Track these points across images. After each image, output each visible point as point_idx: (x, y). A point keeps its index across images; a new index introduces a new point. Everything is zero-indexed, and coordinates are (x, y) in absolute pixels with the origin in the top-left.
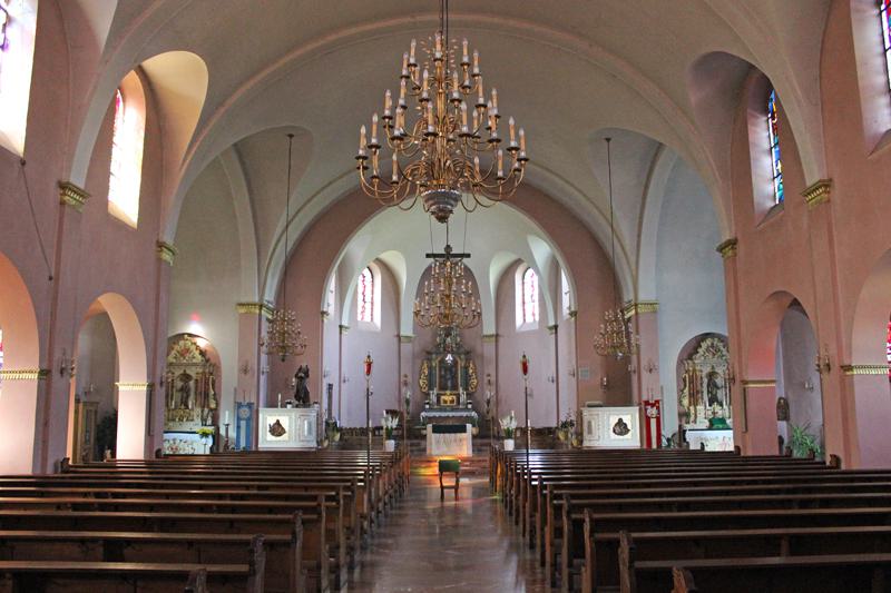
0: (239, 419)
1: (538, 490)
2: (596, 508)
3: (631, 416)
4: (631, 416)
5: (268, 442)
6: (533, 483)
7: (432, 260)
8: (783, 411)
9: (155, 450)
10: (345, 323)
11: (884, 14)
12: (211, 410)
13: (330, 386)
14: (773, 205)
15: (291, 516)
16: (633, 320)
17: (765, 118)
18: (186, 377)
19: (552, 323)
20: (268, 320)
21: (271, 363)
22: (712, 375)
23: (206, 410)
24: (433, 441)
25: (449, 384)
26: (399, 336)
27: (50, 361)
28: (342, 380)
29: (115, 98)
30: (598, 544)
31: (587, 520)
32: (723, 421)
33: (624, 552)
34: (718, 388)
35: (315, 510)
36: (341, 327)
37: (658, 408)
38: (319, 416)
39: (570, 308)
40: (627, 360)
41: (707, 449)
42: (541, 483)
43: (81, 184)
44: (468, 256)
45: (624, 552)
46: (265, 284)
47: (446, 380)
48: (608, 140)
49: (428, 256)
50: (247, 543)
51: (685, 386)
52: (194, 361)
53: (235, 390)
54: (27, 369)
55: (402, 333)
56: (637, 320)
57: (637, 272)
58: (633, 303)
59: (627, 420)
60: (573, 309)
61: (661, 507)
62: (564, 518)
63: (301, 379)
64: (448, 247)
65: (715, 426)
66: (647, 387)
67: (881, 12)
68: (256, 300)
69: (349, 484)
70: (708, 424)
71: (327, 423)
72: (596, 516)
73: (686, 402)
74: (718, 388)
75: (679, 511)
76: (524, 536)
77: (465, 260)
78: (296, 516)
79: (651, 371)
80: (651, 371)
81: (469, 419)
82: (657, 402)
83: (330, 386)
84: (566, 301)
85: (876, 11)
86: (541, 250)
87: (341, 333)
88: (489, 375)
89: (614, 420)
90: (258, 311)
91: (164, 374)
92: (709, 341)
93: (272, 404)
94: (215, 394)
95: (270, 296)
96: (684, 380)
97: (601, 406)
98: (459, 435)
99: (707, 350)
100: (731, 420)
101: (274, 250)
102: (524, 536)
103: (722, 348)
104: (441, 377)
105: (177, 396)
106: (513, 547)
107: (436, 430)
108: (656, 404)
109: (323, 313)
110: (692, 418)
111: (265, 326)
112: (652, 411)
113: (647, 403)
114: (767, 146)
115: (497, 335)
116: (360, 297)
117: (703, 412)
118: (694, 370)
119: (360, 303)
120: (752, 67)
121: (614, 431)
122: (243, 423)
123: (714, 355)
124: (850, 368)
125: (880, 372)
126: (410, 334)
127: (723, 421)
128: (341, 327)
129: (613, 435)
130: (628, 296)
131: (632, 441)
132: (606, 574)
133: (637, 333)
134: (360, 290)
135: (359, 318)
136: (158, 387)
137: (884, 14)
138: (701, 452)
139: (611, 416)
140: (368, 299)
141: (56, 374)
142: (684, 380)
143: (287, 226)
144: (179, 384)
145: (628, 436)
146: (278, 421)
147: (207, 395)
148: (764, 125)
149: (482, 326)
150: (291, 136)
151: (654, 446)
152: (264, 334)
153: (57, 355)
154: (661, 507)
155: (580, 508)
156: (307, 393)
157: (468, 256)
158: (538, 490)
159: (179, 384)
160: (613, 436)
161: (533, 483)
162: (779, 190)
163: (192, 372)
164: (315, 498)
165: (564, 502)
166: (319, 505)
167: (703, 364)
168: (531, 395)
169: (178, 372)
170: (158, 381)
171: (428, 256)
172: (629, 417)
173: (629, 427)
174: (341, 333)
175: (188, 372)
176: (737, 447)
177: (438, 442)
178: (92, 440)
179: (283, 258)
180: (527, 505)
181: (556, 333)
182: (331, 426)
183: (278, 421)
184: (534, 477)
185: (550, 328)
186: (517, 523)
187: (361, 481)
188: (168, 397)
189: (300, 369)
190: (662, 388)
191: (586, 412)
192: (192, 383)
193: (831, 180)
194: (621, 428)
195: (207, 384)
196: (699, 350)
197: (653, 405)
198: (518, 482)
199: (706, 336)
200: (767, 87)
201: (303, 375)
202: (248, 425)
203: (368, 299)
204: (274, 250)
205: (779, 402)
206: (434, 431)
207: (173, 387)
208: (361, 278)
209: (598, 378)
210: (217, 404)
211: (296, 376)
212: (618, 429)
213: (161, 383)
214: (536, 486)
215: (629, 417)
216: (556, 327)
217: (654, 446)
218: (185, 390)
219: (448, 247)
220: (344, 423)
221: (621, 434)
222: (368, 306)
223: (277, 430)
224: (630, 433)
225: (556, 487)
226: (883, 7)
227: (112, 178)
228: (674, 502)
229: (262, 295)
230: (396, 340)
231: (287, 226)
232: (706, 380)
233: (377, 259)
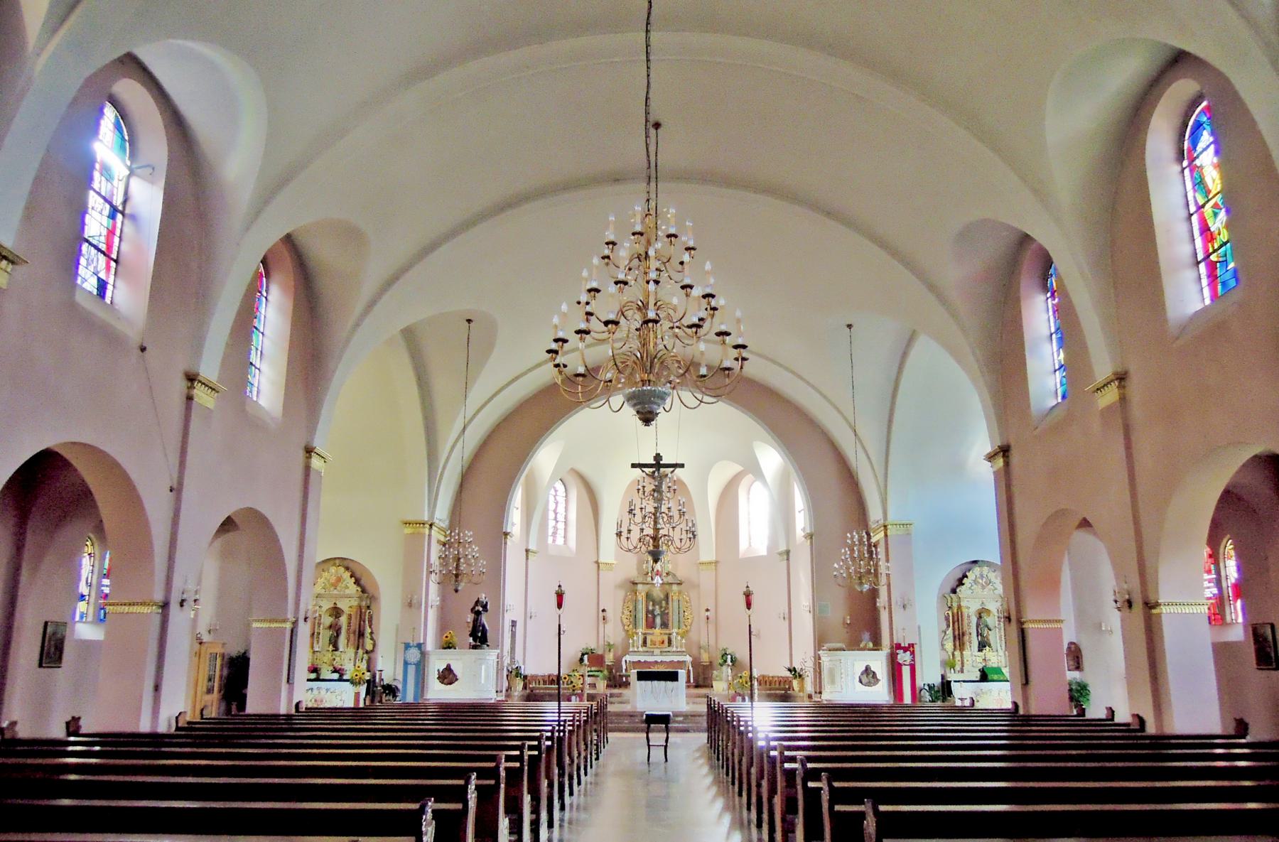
0: (406, 664)
1: (799, 781)
2: (835, 775)
4: (878, 662)
5: (438, 693)
7: (638, 470)
10: (532, 547)
11: (1187, 172)
12: (367, 652)
13: (514, 624)
14: (1054, 403)
17: (1042, 298)
18: (336, 612)
19: (783, 548)
20: (439, 541)
23: (360, 651)
24: (638, 691)
25: (658, 620)
26: (597, 562)
28: (527, 616)
31: (826, 788)
37: (913, 653)
39: (804, 530)
40: (874, 593)
41: (978, 706)
42: (782, 753)
44: (682, 466)
46: (436, 499)
48: (850, 326)
49: (634, 466)
52: (347, 592)
55: (601, 560)
57: (886, 486)
64: (658, 457)
66: (896, 626)
67: (1183, 170)
73: (949, 645)
76: (749, 809)
77: (678, 470)
78: (468, 782)
79: (904, 607)
80: (904, 607)
81: (681, 664)
82: (912, 645)
83: (514, 624)
84: (801, 522)
86: (771, 458)
87: (527, 559)
88: (707, 610)
90: (427, 531)
91: (310, 607)
92: (977, 570)
94: (372, 633)
95: (442, 514)
99: (975, 581)
100: (1007, 669)
101: (448, 458)
102: (749, 809)
104: (648, 612)
105: (325, 635)
106: (726, 808)
107: (643, 676)
108: (910, 648)
109: (506, 534)
110: (958, 667)
112: (903, 657)
113: (899, 646)
114: (1046, 333)
116: (551, 515)
117: (973, 659)
118: (959, 607)
119: (551, 523)
120: (1025, 239)
121: (861, 681)
122: (411, 670)
124: (1157, 605)
125: (145, 610)
128: (527, 551)
131: (880, 694)
132: (813, 830)
134: (552, 506)
135: (550, 540)
136: (301, 622)
137: (1187, 172)
140: (561, 518)
141: (174, 607)
143: (464, 428)
144: (328, 620)
147: (361, 634)
151: (907, 699)
156: (484, 632)
157: (682, 466)
159: (328, 620)
162: (1062, 385)
163: (344, 605)
164: (493, 758)
165: (822, 784)
166: (497, 767)
168: (758, 636)
169: (327, 605)
171: (634, 466)
174: (527, 559)
176: (1015, 705)
179: (459, 469)
180: (777, 800)
181: (788, 559)
182: (516, 673)
185: (780, 554)
189: (477, 602)
190: (919, 627)
191: (826, 659)
192: (343, 620)
193: (1126, 373)
194: (869, 676)
195: (361, 619)
197: (905, 649)
198: (742, 741)
200: (1046, 263)
201: (479, 609)
202: (417, 671)
203: (561, 518)
204: (448, 458)
205: (1069, 648)
207: (319, 624)
208: (552, 492)
209: (838, 613)
210: (374, 645)
212: (865, 679)
213: (306, 619)
216: (788, 552)
217: (907, 699)
218: (336, 629)
219: (658, 457)
220: (528, 670)
221: (868, 684)
222: (561, 526)
223: (447, 676)
225: (810, 759)
226: (1185, 163)
227: (650, 682)
229: (432, 513)
231: (464, 428)
232: (974, 620)
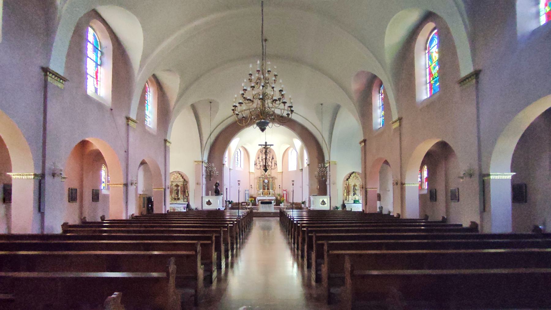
1: (300, 228)
3: (326, 199)
6: (299, 225)
8: (379, 197)
9: (167, 210)
12: (186, 197)
13: (227, 189)
14: (380, 127)
15: (219, 229)
16: (328, 167)
17: (378, 95)
19: (301, 168)
20: (205, 166)
21: (207, 181)
22: (354, 186)
27: (127, 179)
29: (145, 85)
30: (318, 245)
32: (358, 201)
33: (326, 248)
34: (356, 190)
35: (210, 238)
36: (230, 169)
38: (223, 198)
43: (61, 71)
44: (273, 145)
45: (326, 248)
47: (265, 187)
49: (259, 145)
50: (194, 244)
51: (345, 189)
52: (180, 180)
53: (194, 190)
54: (18, 174)
56: (330, 167)
57: (330, 151)
58: (328, 161)
59: (325, 200)
60: (308, 164)
61: (339, 231)
62: (306, 235)
63: (216, 186)
64: (266, 143)
65: (356, 202)
67: (426, 53)
68: (201, 160)
69: (232, 222)
70: (353, 202)
71: (226, 201)
72: (318, 235)
73: (345, 194)
74: (356, 190)
75: (388, 249)
83: (227, 189)
85: (424, 53)
87: (230, 171)
89: (321, 200)
90: (201, 163)
92: (354, 174)
93: (207, 194)
95: (205, 158)
96: (345, 187)
97: (316, 195)
98: (269, 205)
99: (353, 177)
103: (358, 177)
109: (224, 164)
111: (204, 169)
115: (282, 172)
116: (236, 159)
117: (351, 197)
121: (321, 204)
123: (355, 179)
126: (253, 171)
127: (358, 201)
128: (230, 169)
129: (320, 204)
130: (326, 159)
131: (326, 207)
133: (330, 171)
136: (167, 189)
138: (351, 212)
139: (321, 199)
140: (239, 160)
141: (129, 185)
142: (345, 187)
145: (326, 205)
146: (209, 200)
148: (378, 98)
149: (277, 169)
150: (211, 102)
152: (204, 172)
153: (48, 165)
154: (339, 231)
155: (311, 232)
156: (219, 191)
158: (300, 228)
159: (176, 188)
160: (321, 205)
161: (299, 225)
163: (179, 184)
167: (352, 182)
170: (167, 187)
172: (326, 199)
173: (326, 202)
174: (230, 171)
175: (178, 184)
177: (262, 207)
178: (146, 207)
181: (302, 171)
183: (209, 200)
184: (295, 220)
185: (300, 170)
186: (289, 235)
187: (242, 217)
188: (171, 192)
192: (179, 188)
196: (350, 177)
199: (353, 172)
201: (217, 185)
206: (261, 204)
209: (316, 186)
211: (215, 185)
212: (322, 203)
214: (299, 226)
215: (326, 199)
216: (302, 169)
221: (323, 205)
222: (239, 162)
224: (326, 204)
228: (382, 243)
230: (249, 173)
233: (242, 146)
